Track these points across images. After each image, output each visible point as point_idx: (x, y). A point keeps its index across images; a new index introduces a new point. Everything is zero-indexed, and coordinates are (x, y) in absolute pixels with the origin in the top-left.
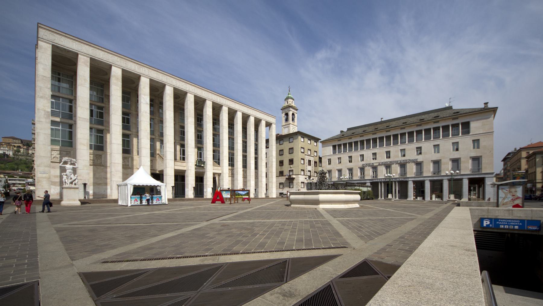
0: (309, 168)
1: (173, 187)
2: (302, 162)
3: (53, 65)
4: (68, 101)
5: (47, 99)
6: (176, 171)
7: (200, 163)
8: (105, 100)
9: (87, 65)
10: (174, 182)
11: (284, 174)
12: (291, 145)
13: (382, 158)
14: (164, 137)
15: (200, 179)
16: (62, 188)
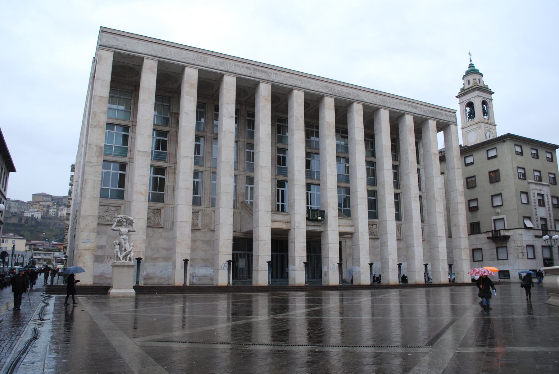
0: (542, 212)
1: (269, 262)
2: (524, 201)
3: (198, 94)
4: (121, 128)
5: (101, 127)
7: (315, 215)
8: (171, 121)
9: (153, 71)
10: (270, 253)
11: (483, 229)
12: (493, 165)
14: (255, 170)
15: (315, 243)
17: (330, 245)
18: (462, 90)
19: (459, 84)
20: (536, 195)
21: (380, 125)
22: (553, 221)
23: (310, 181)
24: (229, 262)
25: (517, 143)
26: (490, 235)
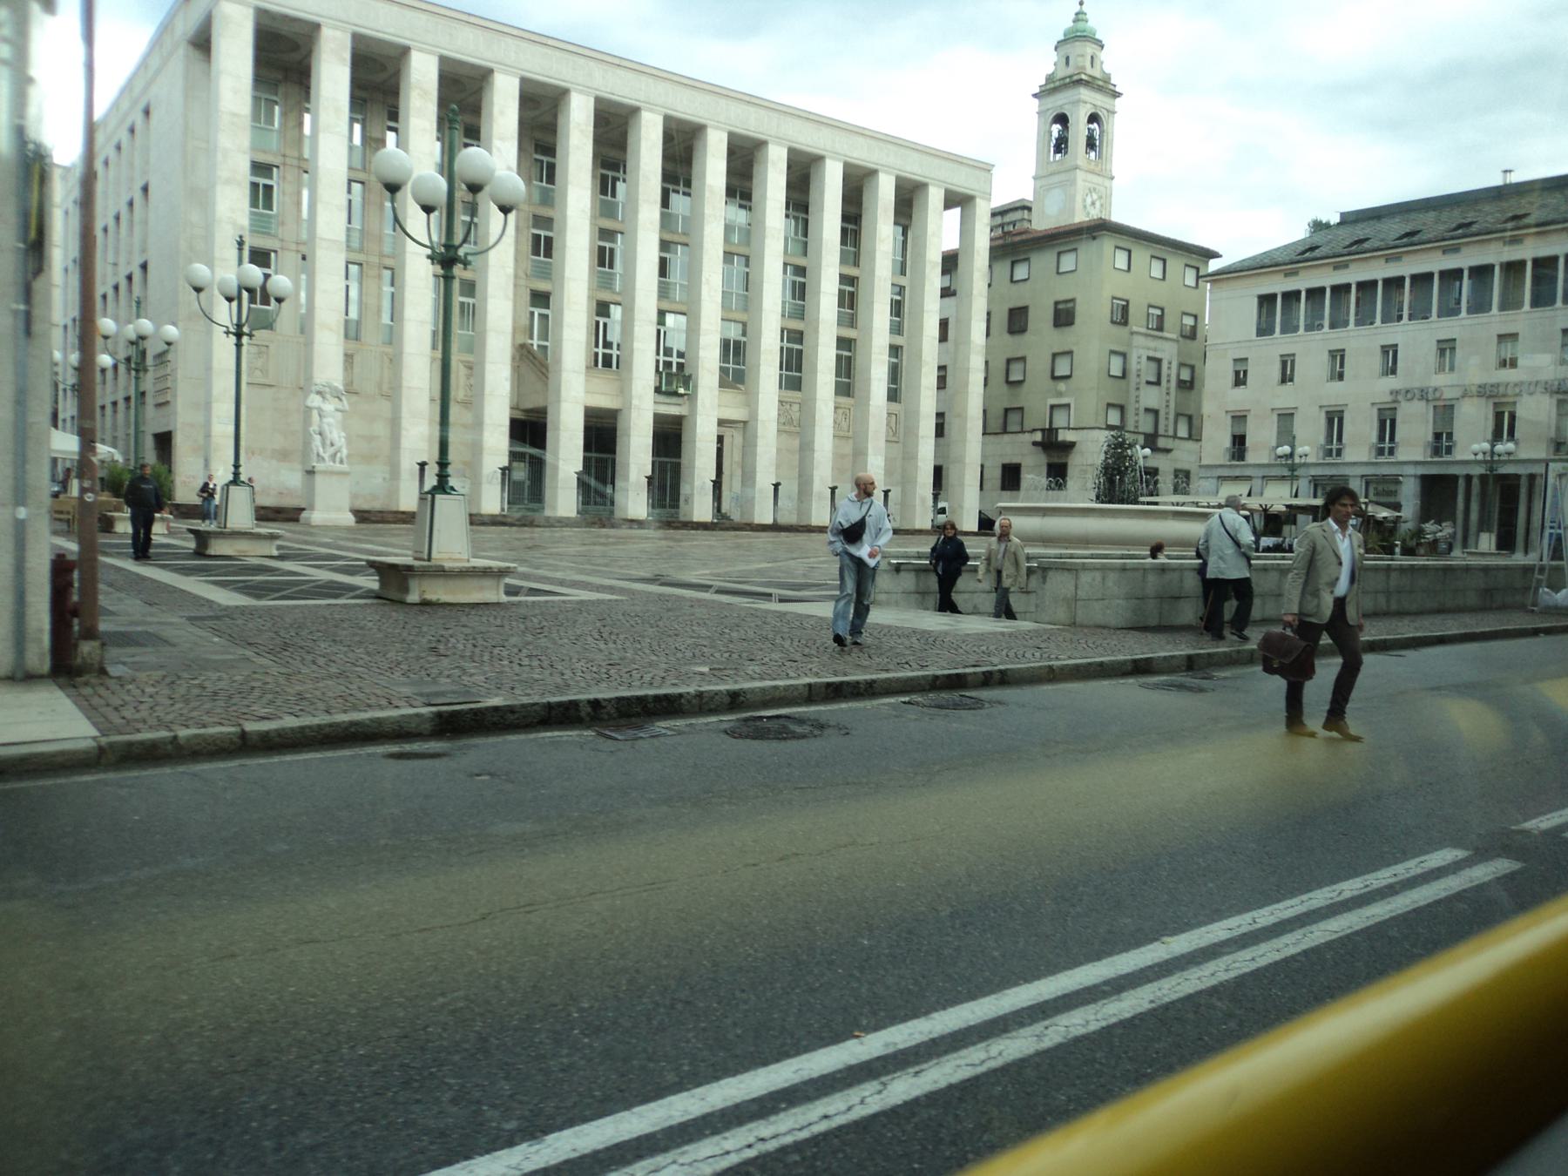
2: (1116, 370)
6: (659, 419)
13: (1476, 368)
15: (670, 439)
16: (311, 472)
17: (698, 444)
18: (1050, 79)
19: (1045, 63)
20: (1144, 359)
21: (822, 193)
22: (1172, 417)
23: (665, 306)
24: (503, 469)
25: (1121, 244)
26: (1038, 437)
